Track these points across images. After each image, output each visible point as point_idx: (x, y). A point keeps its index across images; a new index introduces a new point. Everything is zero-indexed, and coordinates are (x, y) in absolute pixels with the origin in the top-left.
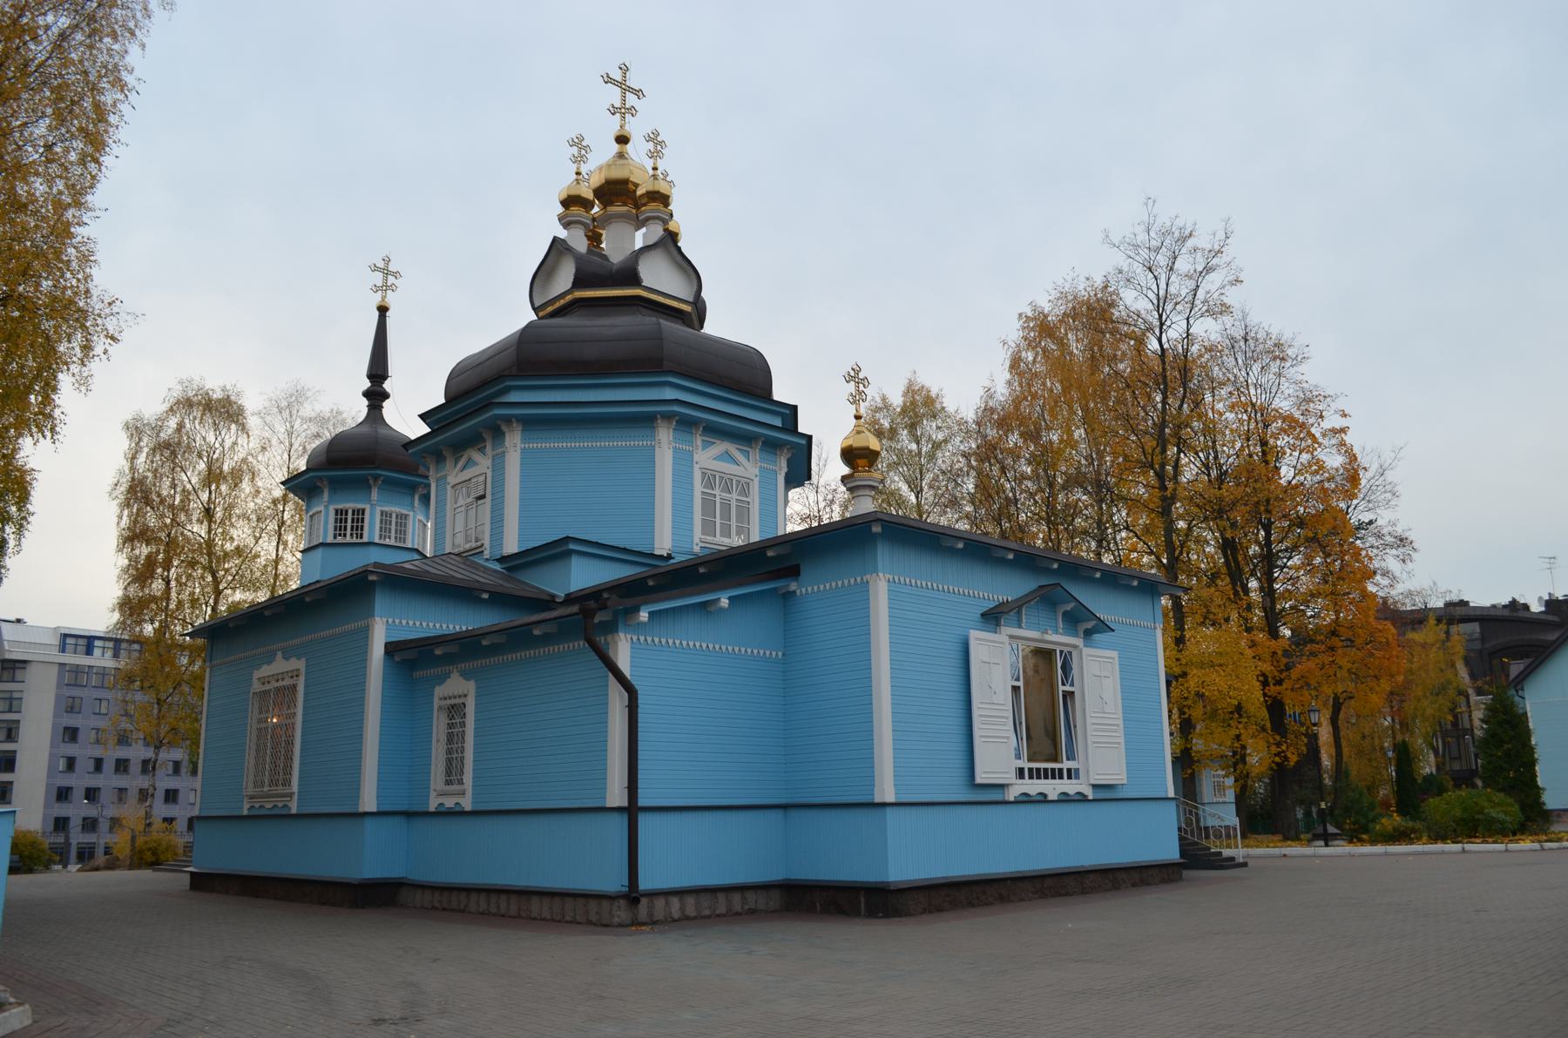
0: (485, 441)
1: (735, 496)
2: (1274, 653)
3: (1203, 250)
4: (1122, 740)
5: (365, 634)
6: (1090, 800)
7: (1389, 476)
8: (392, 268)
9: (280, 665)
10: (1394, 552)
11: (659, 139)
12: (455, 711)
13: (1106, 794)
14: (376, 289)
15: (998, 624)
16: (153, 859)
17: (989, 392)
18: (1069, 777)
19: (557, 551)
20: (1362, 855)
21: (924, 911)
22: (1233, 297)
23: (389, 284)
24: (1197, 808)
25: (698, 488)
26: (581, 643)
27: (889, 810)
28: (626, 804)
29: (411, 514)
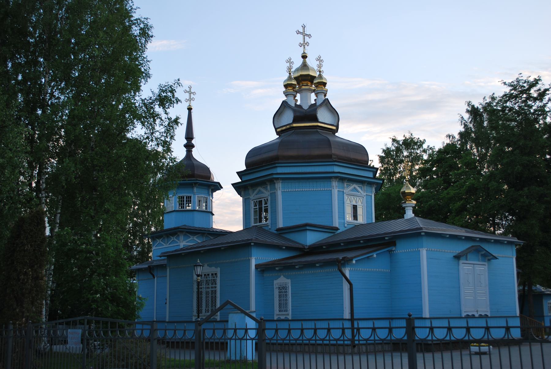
0: (267, 185)
5: (249, 261)
12: (283, 289)
19: (302, 228)
23: (191, 98)
26: (336, 269)
29: (208, 197)
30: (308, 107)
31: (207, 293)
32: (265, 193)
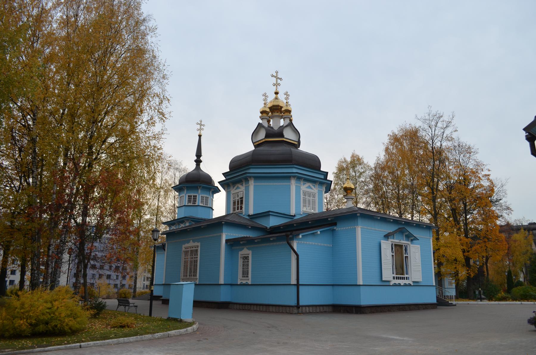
0: (243, 182)
1: (311, 198)
2: (467, 243)
3: (446, 121)
4: (421, 269)
5: (220, 237)
6: (250, 285)
7: (505, 188)
8: (202, 123)
9: (191, 244)
10: (505, 212)
11: (288, 94)
12: (246, 258)
13: (416, 284)
14: (198, 130)
15: (388, 238)
16: (124, 296)
17: (378, 159)
18: (407, 279)
19: (266, 214)
20: (491, 304)
21: (370, 313)
22: (454, 136)
24: (442, 289)
25: (302, 196)
27: (361, 286)
28: (296, 283)
29: (209, 197)
30: (277, 128)
31: (191, 262)
32: (242, 188)
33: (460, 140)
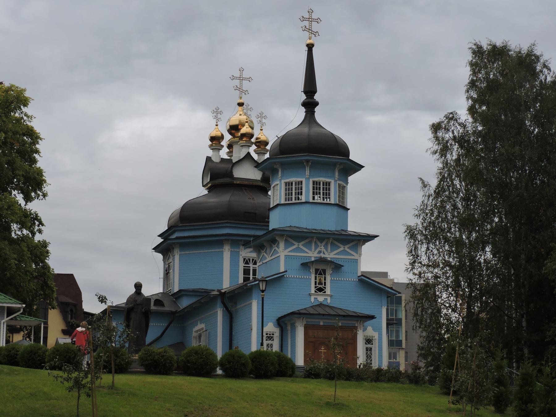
8: (314, 16)
25: (242, 265)
33: (39, 155)
